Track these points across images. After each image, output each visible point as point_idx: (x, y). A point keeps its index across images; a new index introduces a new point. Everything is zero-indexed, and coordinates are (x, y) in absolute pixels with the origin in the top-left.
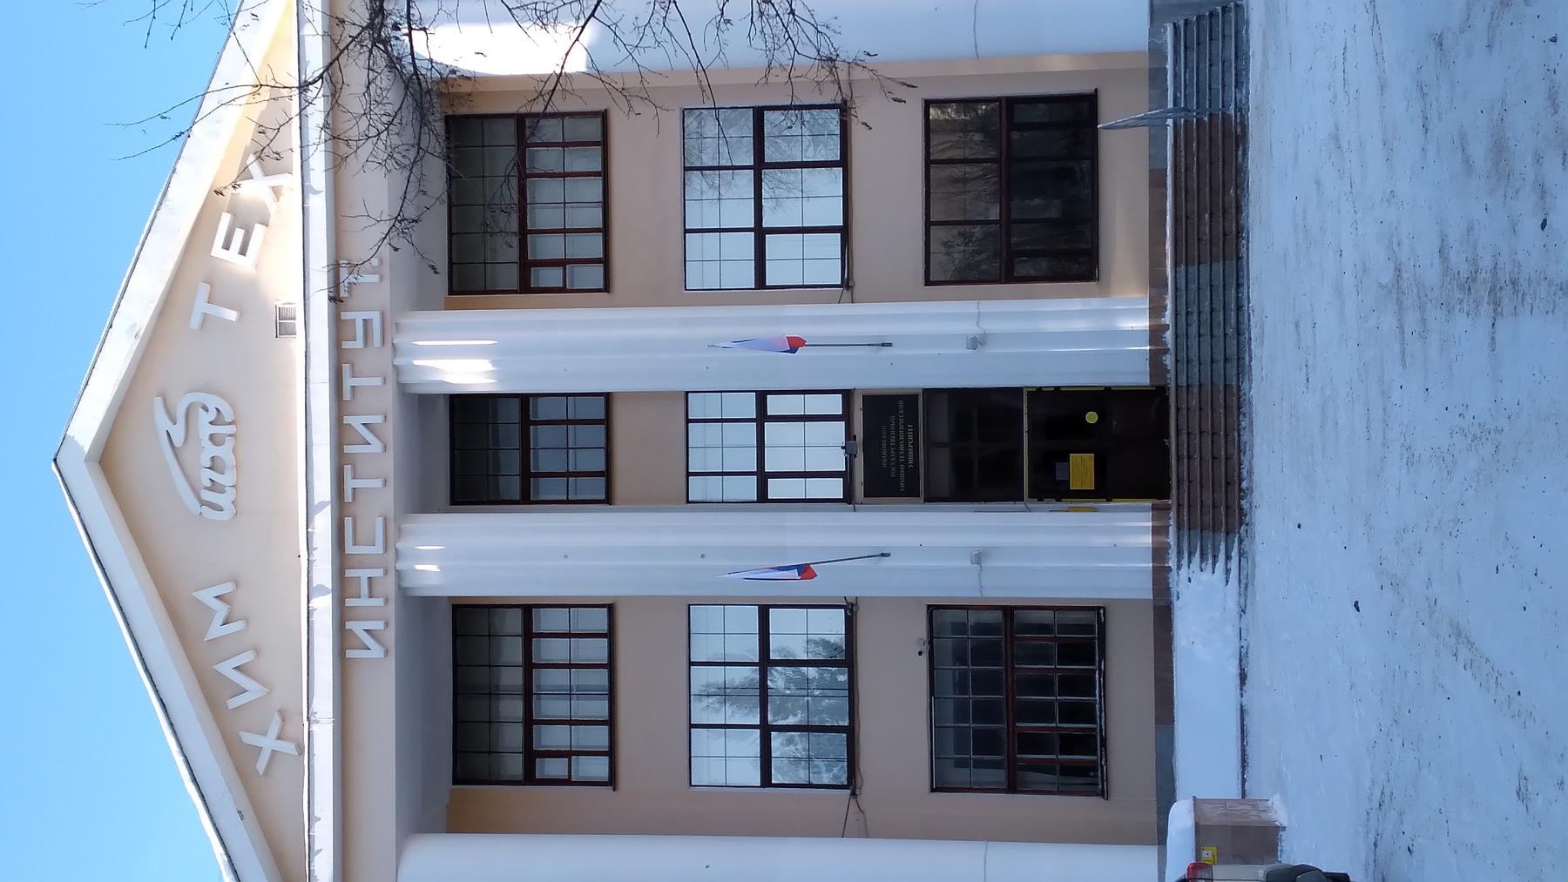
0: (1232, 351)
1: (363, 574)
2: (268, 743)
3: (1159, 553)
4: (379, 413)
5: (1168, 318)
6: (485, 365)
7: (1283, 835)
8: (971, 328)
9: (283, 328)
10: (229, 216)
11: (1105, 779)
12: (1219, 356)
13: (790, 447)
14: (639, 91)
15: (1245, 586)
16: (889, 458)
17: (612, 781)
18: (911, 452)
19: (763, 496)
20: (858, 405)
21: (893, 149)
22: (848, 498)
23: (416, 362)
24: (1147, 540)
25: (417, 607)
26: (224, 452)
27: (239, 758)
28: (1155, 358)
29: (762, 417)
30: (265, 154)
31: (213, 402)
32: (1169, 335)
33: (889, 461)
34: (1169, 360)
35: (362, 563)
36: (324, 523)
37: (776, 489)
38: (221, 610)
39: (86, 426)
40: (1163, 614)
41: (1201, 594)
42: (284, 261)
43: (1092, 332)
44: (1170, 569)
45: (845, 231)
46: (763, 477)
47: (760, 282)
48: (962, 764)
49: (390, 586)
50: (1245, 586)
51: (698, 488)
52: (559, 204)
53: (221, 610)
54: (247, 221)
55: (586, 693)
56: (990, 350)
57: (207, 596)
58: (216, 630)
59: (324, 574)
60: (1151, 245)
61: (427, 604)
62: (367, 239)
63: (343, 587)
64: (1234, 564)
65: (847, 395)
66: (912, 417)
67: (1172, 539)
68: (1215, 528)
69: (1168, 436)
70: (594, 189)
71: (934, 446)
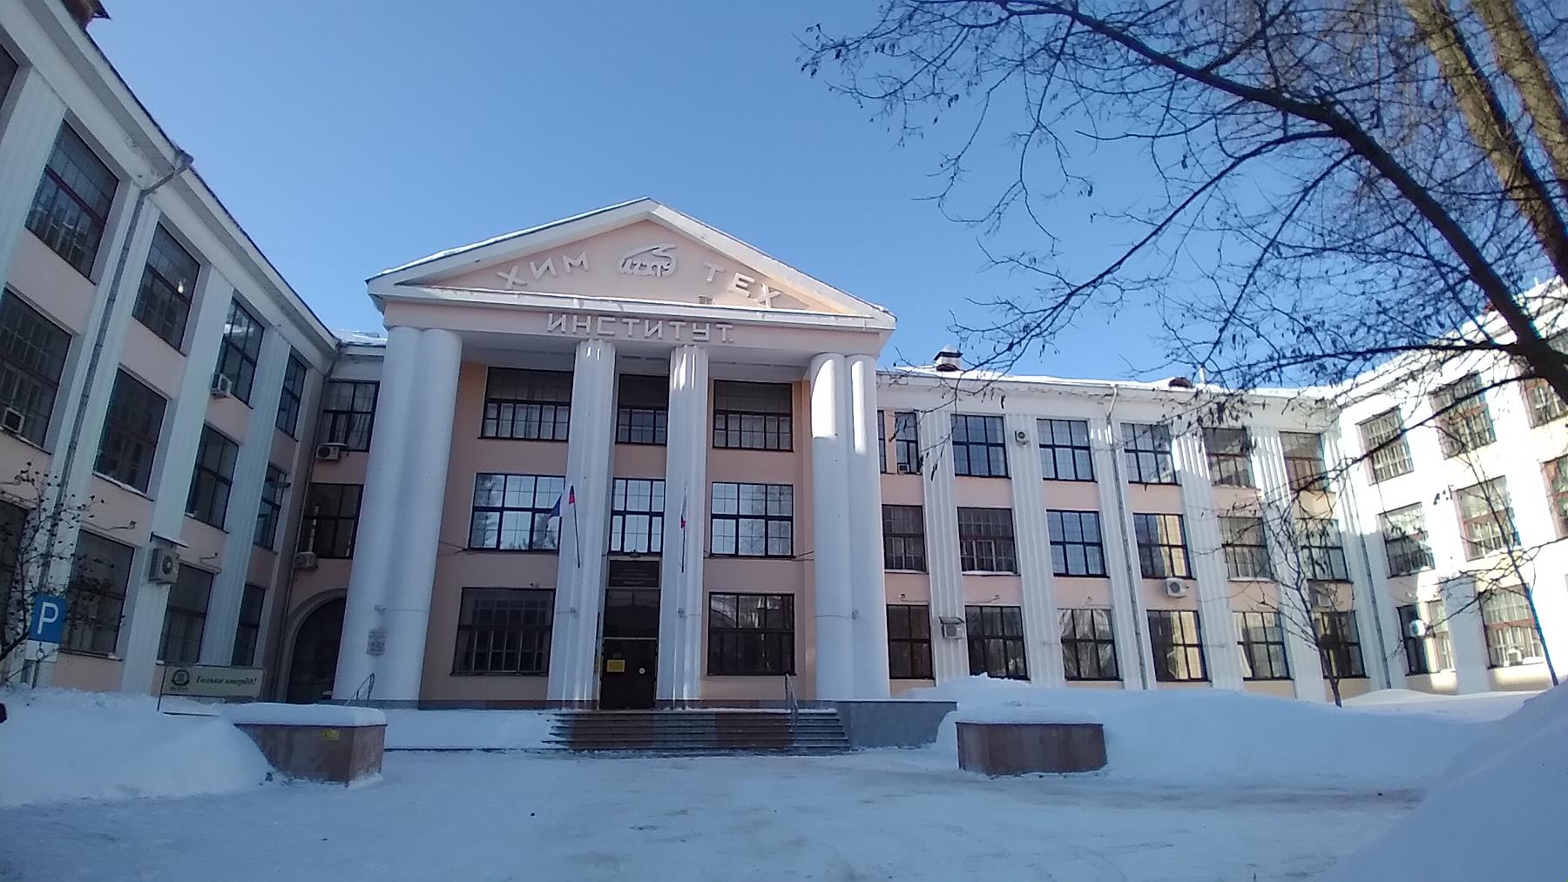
0: (670, 745)
1: (588, 324)
2: (511, 278)
3: (570, 703)
4: (664, 336)
5: (688, 709)
6: (682, 382)
7: (342, 786)
8: (688, 612)
9: (702, 300)
10: (753, 280)
11: (460, 674)
12: (668, 738)
13: (637, 525)
14: (804, 468)
15: (540, 753)
17: (483, 437)
19: (614, 513)
20: (656, 559)
21: (772, 579)
22: (610, 552)
25: (569, 351)
26: (649, 270)
27: (507, 265)
28: (669, 702)
29: (652, 514)
30: (778, 298)
31: (673, 264)
32: (680, 710)
34: (667, 710)
35: (593, 323)
36: (615, 308)
37: (618, 519)
38: (577, 263)
39: (664, 213)
40: (541, 705)
41: (539, 726)
42: (732, 302)
43: (683, 672)
45: (736, 556)
46: (624, 513)
47: (714, 516)
48: (476, 603)
49: (581, 335)
50: (540, 753)
51: (620, 484)
52: (752, 430)
53: (577, 263)
54: (751, 289)
55: (527, 427)
56: (678, 621)
57: (583, 257)
58: (567, 260)
59: (588, 306)
62: (743, 340)
63: (582, 314)
64: (553, 745)
65: (660, 554)
67: (577, 710)
68: (573, 736)
70: (758, 444)
71: (633, 585)
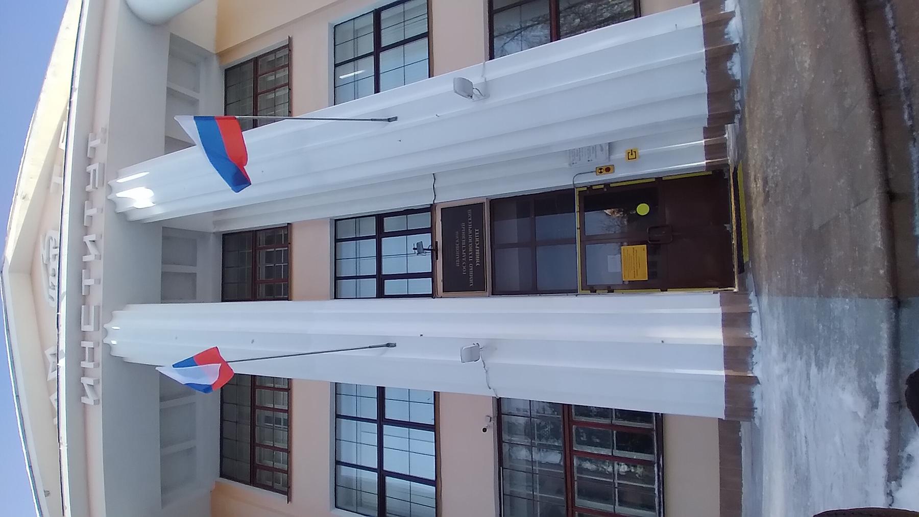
16: (461, 257)
18: (478, 253)
23: (119, 195)
24: (715, 336)
29: (381, 234)
33: (461, 263)
44: (755, 381)
46: (381, 278)
60: (723, 483)
61: (121, 362)
66: (479, 223)
69: (729, 221)
